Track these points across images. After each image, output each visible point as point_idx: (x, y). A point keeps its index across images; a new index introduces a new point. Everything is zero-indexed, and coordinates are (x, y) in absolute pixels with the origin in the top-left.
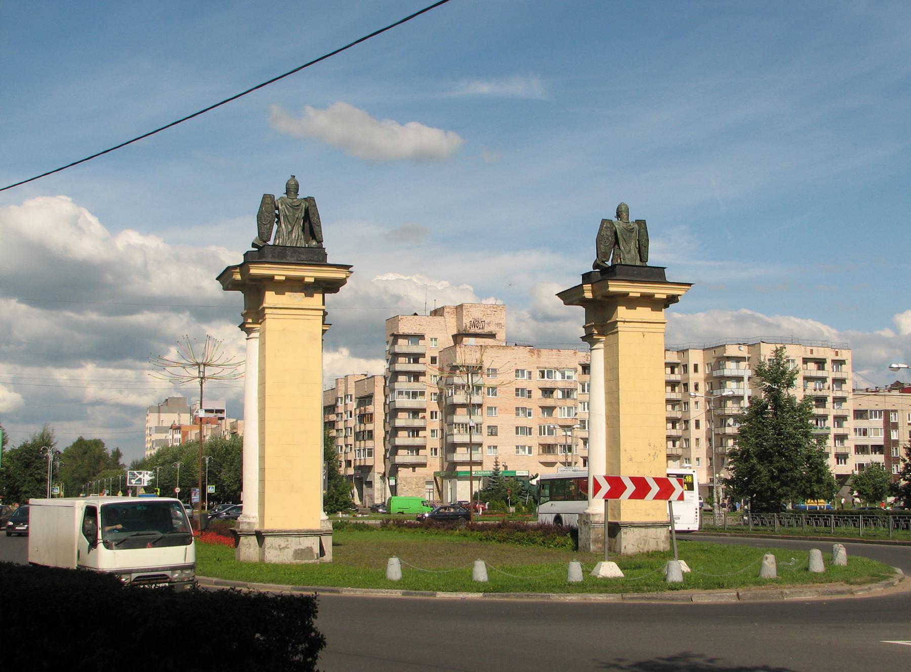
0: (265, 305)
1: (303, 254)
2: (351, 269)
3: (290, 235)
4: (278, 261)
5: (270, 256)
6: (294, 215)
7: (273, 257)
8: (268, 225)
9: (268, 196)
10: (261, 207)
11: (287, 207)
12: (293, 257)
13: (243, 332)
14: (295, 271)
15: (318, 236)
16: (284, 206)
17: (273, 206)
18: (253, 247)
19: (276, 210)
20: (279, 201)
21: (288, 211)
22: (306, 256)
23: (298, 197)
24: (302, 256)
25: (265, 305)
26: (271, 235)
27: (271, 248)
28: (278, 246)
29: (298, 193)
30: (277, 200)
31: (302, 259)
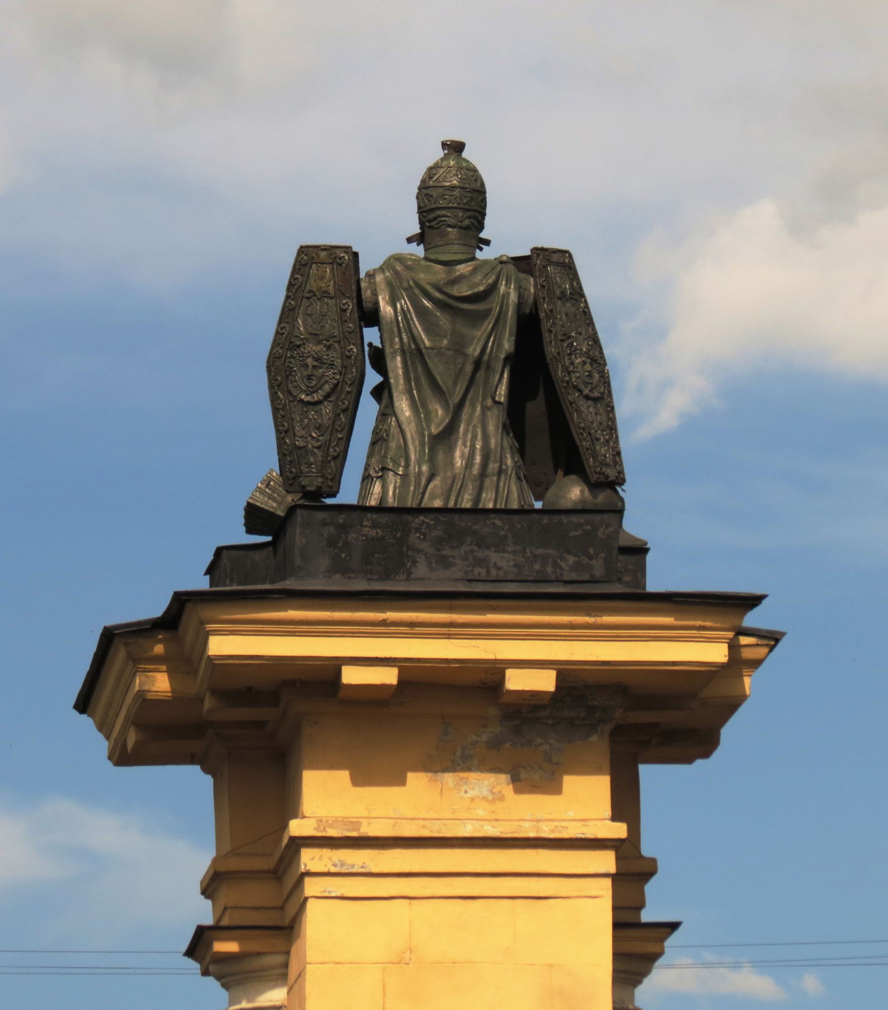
0: (297, 828)
1: (499, 545)
2: (752, 619)
3: (440, 456)
4: (359, 585)
5: (324, 563)
6: (459, 347)
7: (340, 567)
8: (327, 409)
9: (323, 254)
10: (288, 313)
11: (421, 312)
12: (445, 562)
13: (211, 980)
14: (449, 636)
15: (595, 455)
16: (405, 303)
17: (351, 305)
18: (251, 529)
19: (369, 325)
20: (379, 278)
21: (427, 330)
22: (520, 559)
23: (484, 254)
24: (494, 557)
25: (297, 828)
26: (341, 458)
27: (325, 524)
28: (380, 509)
29: (483, 235)
30: (371, 275)
31: (494, 573)
